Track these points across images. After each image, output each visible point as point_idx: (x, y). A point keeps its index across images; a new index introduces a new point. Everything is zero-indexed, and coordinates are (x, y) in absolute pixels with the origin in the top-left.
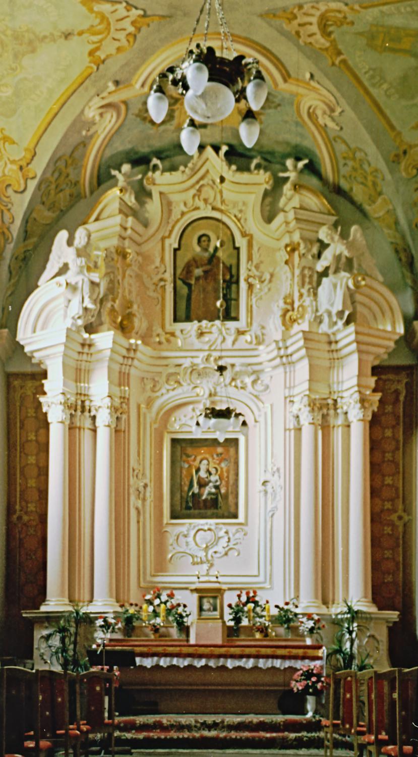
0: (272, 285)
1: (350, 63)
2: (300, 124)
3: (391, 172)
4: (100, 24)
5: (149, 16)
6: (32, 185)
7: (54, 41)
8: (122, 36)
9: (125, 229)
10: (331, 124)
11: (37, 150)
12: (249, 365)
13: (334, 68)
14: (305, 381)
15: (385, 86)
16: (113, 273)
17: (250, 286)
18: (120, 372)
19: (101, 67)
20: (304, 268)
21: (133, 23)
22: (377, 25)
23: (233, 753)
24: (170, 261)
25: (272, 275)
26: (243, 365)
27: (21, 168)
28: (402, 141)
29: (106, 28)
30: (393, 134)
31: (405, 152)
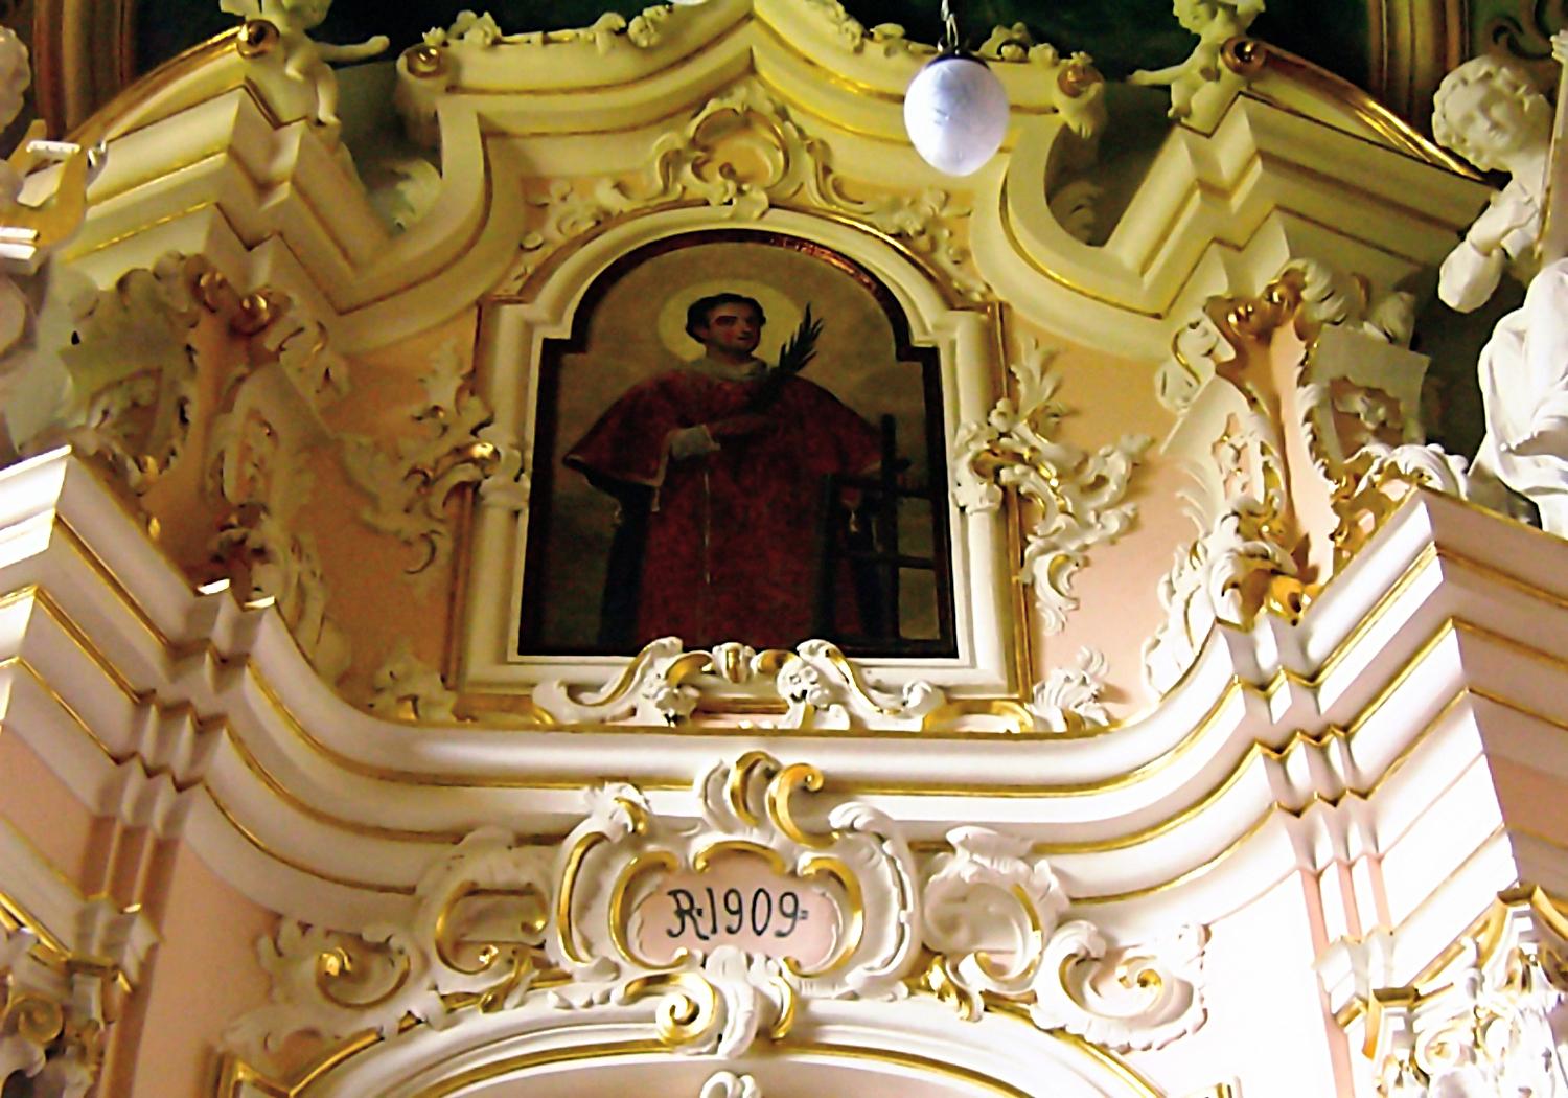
0: (1146, 506)
9: (264, 187)
12: (1043, 846)
14: (1479, 756)
16: (155, 374)
17: (1013, 510)
18: (101, 824)
20: (1338, 389)
23: (562, 882)
24: (523, 387)
25: (1139, 466)
26: (1000, 840)
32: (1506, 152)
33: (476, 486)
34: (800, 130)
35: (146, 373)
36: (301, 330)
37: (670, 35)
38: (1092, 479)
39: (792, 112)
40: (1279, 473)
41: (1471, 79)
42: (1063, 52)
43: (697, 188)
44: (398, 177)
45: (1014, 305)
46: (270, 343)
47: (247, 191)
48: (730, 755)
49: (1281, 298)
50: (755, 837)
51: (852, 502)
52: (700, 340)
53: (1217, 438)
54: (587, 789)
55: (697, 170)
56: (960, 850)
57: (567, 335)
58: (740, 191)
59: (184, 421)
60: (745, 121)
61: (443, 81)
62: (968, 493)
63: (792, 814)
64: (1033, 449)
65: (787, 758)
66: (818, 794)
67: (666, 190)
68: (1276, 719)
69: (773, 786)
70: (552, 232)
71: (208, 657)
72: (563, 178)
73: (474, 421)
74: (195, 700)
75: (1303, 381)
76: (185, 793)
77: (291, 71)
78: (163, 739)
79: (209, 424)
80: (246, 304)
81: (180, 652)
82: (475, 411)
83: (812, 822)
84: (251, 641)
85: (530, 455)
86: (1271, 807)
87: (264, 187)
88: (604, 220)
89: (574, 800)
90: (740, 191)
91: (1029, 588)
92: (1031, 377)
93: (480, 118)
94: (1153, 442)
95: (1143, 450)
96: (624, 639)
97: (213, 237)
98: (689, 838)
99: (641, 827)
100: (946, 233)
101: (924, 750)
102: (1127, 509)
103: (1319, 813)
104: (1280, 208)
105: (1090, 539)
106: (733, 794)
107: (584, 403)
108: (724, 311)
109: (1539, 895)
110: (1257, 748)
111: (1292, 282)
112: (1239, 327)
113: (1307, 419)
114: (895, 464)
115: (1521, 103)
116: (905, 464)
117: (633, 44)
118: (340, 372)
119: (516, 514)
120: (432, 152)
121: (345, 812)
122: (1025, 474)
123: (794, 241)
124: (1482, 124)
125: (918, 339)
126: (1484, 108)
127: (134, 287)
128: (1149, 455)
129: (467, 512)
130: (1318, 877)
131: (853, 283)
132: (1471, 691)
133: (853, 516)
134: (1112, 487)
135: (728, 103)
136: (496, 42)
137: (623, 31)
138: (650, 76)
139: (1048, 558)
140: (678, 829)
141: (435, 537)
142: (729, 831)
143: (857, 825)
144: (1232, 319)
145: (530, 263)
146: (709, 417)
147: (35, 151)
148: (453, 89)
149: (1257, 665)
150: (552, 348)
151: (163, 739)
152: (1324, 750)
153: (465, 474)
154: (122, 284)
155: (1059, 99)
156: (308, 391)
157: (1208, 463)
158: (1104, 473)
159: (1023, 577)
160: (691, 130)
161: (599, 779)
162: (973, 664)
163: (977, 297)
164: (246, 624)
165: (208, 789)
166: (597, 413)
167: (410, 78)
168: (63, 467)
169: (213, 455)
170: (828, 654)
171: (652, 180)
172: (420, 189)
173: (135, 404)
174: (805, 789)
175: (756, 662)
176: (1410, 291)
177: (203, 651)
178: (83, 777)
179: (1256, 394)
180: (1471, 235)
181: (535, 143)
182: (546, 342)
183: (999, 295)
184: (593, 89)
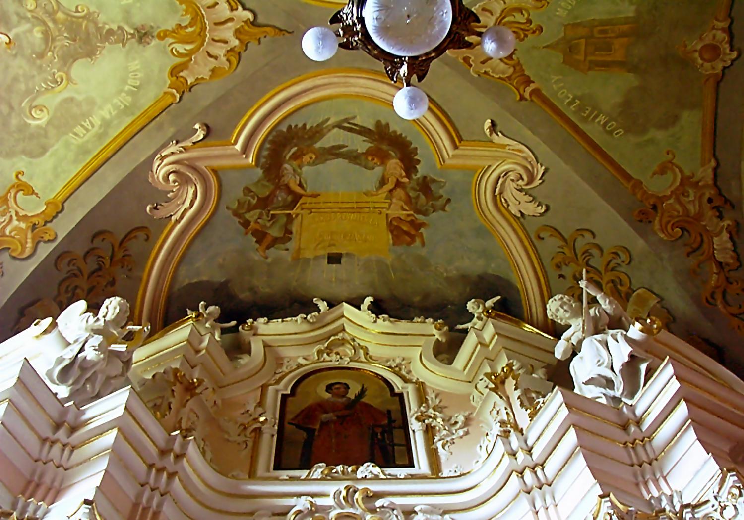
1: (544, 92)
2: (484, 232)
3: (642, 235)
4: (191, 25)
5: (259, 26)
6: (45, 251)
7: (123, 42)
8: (220, 51)
9: (198, 351)
10: (531, 209)
11: (66, 204)
13: (523, 102)
15: (602, 119)
16: (162, 397)
17: (430, 432)
18: (136, 505)
19: (187, 95)
20: (526, 392)
21: (238, 33)
22: (575, 26)
27: (34, 227)
28: (645, 192)
29: (199, 34)
30: (629, 186)
31: (655, 207)
32: (569, 318)
33: (260, 429)
34: (359, 344)
35: (160, 397)
36: (207, 388)
37: (319, 320)
38: (453, 422)
39: (356, 339)
40: (511, 414)
41: (557, 299)
42: (435, 320)
43: (328, 358)
44: (237, 358)
45: (426, 383)
46: (198, 391)
47: (193, 352)
48: (341, 486)
49: (507, 370)
50: (351, 510)
51: (379, 430)
52: (330, 393)
53: (491, 409)
54: (295, 498)
55: (328, 354)
56: (419, 513)
57: (289, 392)
58: (341, 358)
59: (170, 408)
60: (343, 342)
61: (252, 332)
62: (415, 426)
63: (363, 503)
64: (434, 414)
65: (360, 487)
66: (371, 497)
67: (319, 359)
68: (519, 463)
69: (357, 495)
70: (285, 369)
71: (172, 454)
72: (287, 357)
73: (260, 413)
74: (167, 467)
75: (516, 389)
76: (164, 497)
77: (207, 325)
78: (157, 479)
79: (178, 411)
80: (191, 381)
81: (163, 453)
82: (260, 410)
83: (370, 505)
84: (187, 449)
85: (277, 421)
86: (520, 491)
87: (198, 351)
88: (300, 366)
89: (292, 501)
90: (341, 358)
91: (436, 450)
92: (432, 398)
93: (263, 341)
94: (471, 413)
95: (470, 414)
96: (307, 465)
97: (181, 364)
98: (330, 512)
99: (313, 508)
100: (404, 367)
101: (406, 484)
102: (465, 429)
103: (536, 492)
104: (503, 347)
105: (454, 437)
106: (344, 497)
107: (295, 407)
108: (337, 386)
109: (611, 495)
110: (514, 473)
111: (510, 366)
112: (495, 379)
113: (518, 398)
114: (391, 421)
115: (572, 305)
116: (394, 421)
117: (308, 322)
118: (219, 402)
119: (273, 436)
120: (249, 352)
121: (218, 507)
122: (432, 421)
123: (357, 369)
124: (561, 310)
125: (397, 391)
126: (562, 306)
127: (157, 377)
128: (470, 416)
129: (257, 436)
130: (537, 513)
131: (376, 379)
132: (581, 447)
133: (379, 434)
134: (460, 424)
135: (337, 337)
136: (268, 322)
137: (305, 319)
138: (313, 331)
139: (442, 442)
140: (326, 509)
141: (248, 442)
142: (342, 509)
143: (385, 505)
144: (493, 377)
145: (278, 376)
146: (334, 411)
147: (129, 329)
148: (255, 335)
149: (512, 449)
150: (284, 397)
151: (157, 479)
152: (535, 473)
153: (258, 425)
154: (154, 376)
155: (435, 332)
156: (209, 404)
157: (489, 417)
158: (457, 420)
159: (433, 446)
160: (326, 345)
161: (299, 495)
162: (420, 468)
163: (414, 381)
164: (184, 446)
165: (170, 495)
166: (298, 411)
167: (243, 331)
168: (129, 391)
169: (179, 418)
170: (373, 466)
171: (314, 358)
172: (244, 360)
173: (155, 405)
174: (367, 496)
175: (350, 469)
176: (546, 369)
177: (171, 452)
178: (131, 490)
179: (502, 395)
180: (562, 337)
181: (280, 348)
182: (283, 395)
183: (420, 380)
184: (296, 334)
